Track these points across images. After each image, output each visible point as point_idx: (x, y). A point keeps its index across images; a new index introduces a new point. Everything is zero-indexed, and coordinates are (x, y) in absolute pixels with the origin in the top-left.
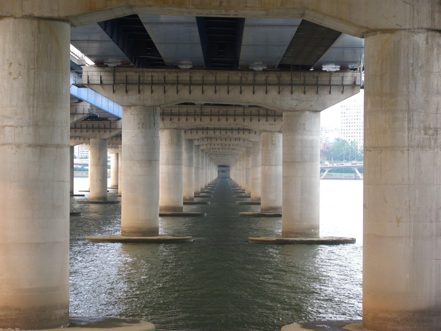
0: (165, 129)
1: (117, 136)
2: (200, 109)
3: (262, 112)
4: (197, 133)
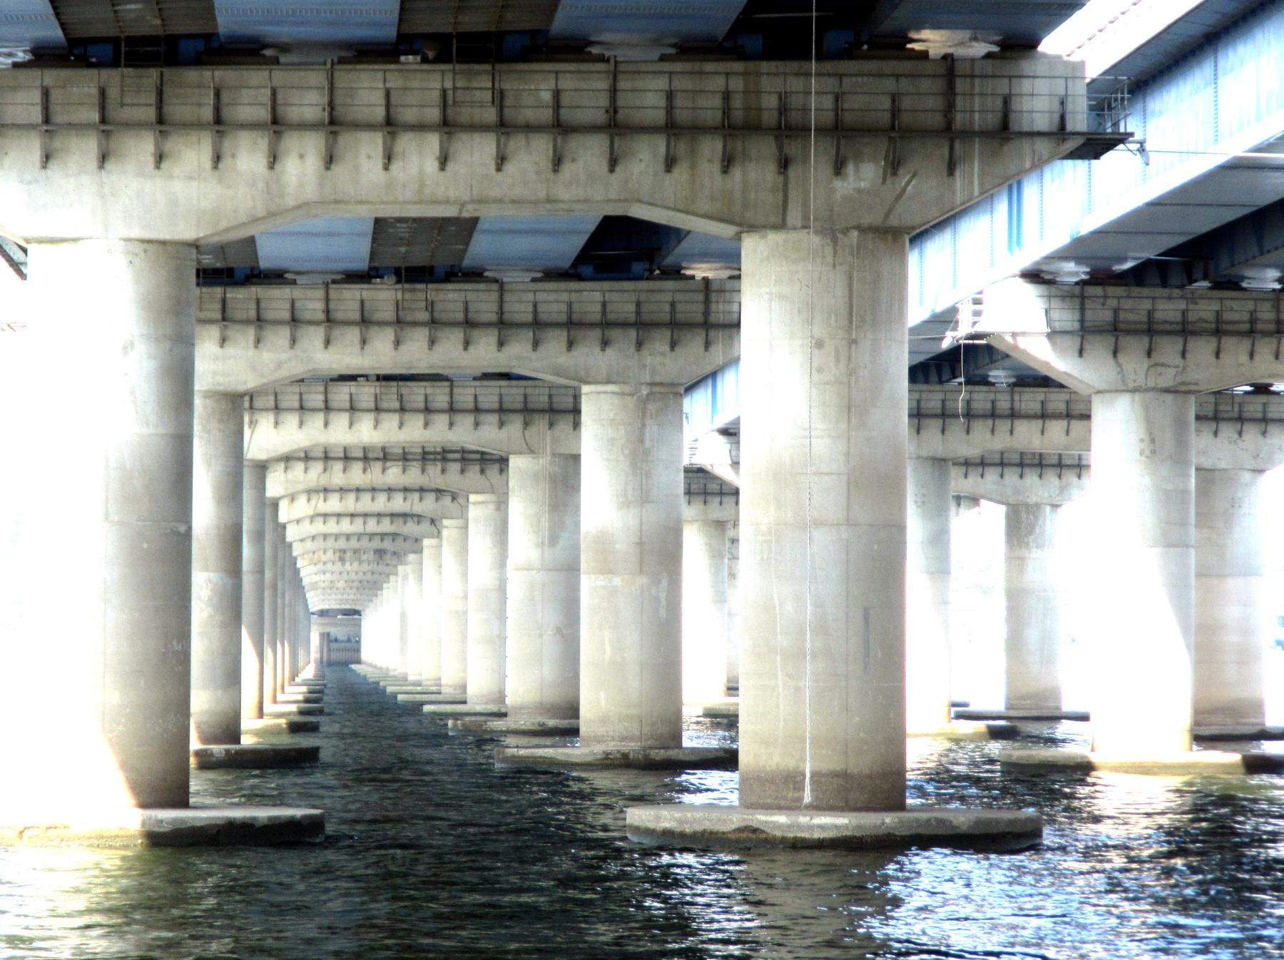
0: (1124, 391)
1: (466, 456)
2: (1273, 307)
3: (540, 399)
4: (968, 432)
